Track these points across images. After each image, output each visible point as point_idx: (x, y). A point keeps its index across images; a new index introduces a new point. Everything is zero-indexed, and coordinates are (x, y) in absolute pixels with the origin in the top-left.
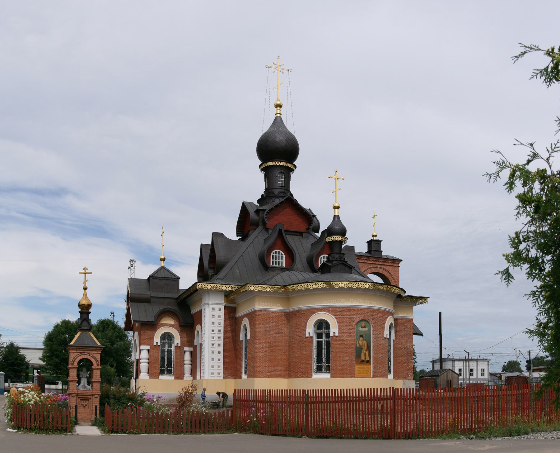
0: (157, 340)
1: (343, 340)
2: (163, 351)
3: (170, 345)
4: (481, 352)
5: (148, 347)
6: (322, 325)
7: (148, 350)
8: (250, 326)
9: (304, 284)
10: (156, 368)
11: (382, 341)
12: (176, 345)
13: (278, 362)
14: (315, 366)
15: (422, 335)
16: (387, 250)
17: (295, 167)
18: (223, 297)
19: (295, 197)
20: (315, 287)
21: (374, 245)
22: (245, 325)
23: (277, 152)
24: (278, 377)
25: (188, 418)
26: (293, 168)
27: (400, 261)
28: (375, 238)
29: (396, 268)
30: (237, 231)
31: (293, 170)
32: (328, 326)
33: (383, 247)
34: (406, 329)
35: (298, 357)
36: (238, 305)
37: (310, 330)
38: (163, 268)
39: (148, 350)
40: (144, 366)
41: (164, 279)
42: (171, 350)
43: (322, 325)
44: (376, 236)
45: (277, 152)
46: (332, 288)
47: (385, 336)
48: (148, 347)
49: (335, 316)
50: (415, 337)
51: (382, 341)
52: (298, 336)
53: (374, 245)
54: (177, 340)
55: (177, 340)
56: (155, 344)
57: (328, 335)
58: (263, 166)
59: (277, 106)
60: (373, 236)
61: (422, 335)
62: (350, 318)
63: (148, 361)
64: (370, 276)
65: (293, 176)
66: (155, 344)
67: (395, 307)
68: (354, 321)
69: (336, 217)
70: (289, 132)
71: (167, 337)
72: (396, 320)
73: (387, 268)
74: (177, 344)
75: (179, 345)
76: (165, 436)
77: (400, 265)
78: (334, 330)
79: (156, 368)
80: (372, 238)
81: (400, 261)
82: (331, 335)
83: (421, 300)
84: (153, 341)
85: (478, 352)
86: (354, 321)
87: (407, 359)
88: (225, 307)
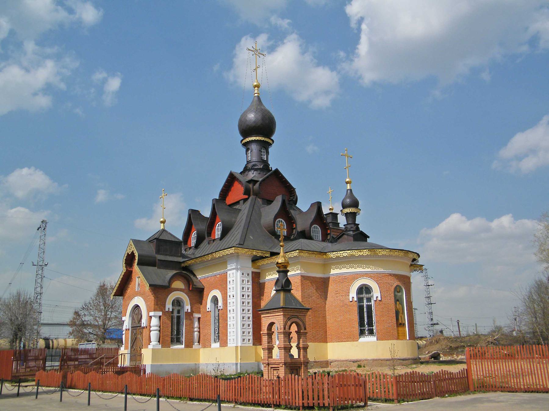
0: (169, 306)
2: (172, 318)
3: (369, 300)
6: (364, 290)
9: (350, 251)
20: (361, 254)
24: (320, 342)
25: (211, 388)
35: (341, 321)
36: (262, 270)
37: (353, 294)
38: (164, 230)
39: (160, 317)
40: (154, 335)
43: (364, 290)
46: (376, 255)
52: (340, 300)
54: (188, 308)
56: (167, 310)
58: (244, 142)
60: (330, 209)
62: (389, 284)
66: (167, 310)
68: (392, 286)
71: (178, 303)
74: (377, 297)
75: (379, 298)
78: (376, 293)
84: (165, 307)
88: (252, 272)
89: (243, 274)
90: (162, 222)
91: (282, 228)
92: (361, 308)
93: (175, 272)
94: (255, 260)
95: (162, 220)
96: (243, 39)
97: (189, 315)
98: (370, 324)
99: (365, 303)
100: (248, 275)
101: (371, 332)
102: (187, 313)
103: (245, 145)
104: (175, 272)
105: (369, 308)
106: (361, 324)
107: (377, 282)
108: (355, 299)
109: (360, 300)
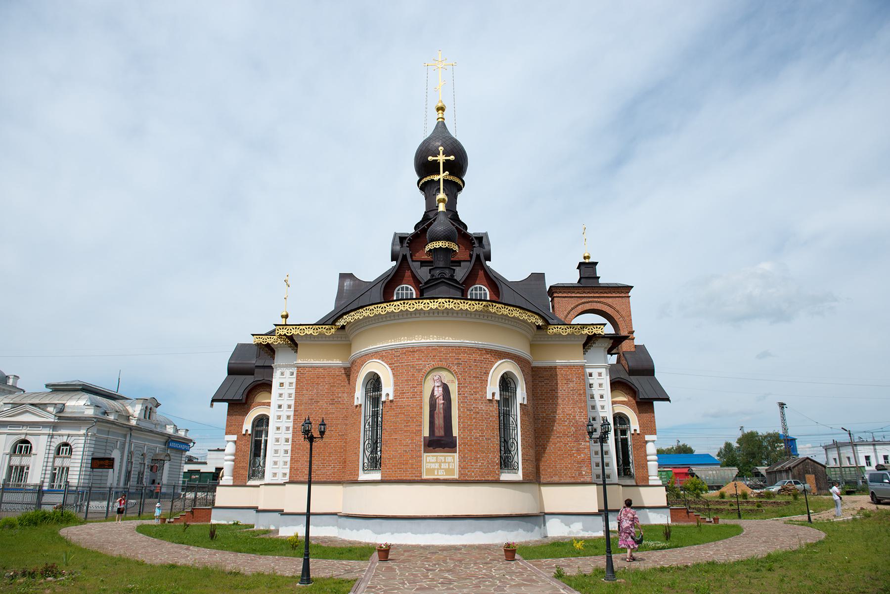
1: (401, 407)
5: (234, 438)
7: (235, 442)
10: (243, 468)
11: (483, 407)
12: (633, 432)
13: (330, 453)
14: (363, 458)
15: (668, 399)
16: (605, 276)
23: (442, 166)
26: (460, 183)
28: (587, 261)
29: (624, 300)
33: (599, 271)
34: (571, 385)
37: (359, 395)
39: (235, 442)
42: (627, 439)
44: (589, 257)
45: (442, 166)
48: (234, 438)
49: (390, 364)
51: (483, 407)
59: (438, 109)
60: (585, 258)
61: (668, 399)
63: (233, 458)
70: (453, 138)
73: (609, 301)
76: (414, 543)
77: (630, 294)
78: (388, 390)
79: (243, 468)
80: (583, 260)
86: (420, 370)
87: (577, 441)
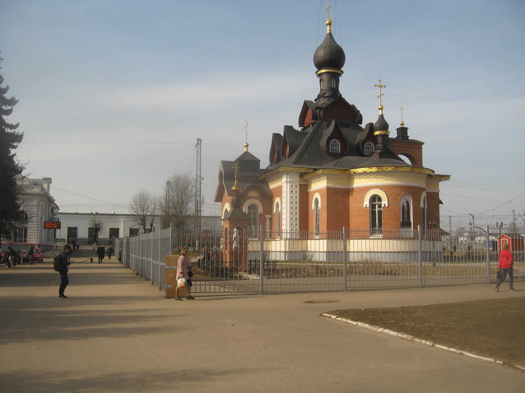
4: (483, 215)
8: (321, 199)
16: (412, 135)
17: (343, 72)
18: (298, 176)
19: (343, 96)
21: (403, 131)
22: (317, 199)
27: (423, 143)
30: (299, 123)
31: (340, 75)
32: (380, 199)
37: (366, 203)
38: (247, 153)
41: (248, 162)
43: (375, 198)
47: (421, 207)
50: (440, 205)
53: (403, 131)
54: (260, 210)
55: (260, 210)
57: (380, 206)
58: (319, 72)
64: (401, 156)
65: (341, 79)
67: (427, 183)
69: (382, 117)
71: (253, 207)
72: (427, 193)
75: (262, 213)
78: (385, 202)
81: (423, 143)
82: (383, 206)
83: (446, 177)
85: (480, 215)
89: (292, 186)
90: (379, 109)
91: (337, 146)
92: (373, 213)
93: (248, 185)
94: (302, 175)
95: (380, 107)
96: (13, 151)
97: (262, 216)
98: (380, 225)
99: (377, 209)
100: (296, 186)
101: (380, 232)
102: (260, 214)
103: (319, 75)
104: (248, 185)
105: (380, 212)
106: (373, 225)
107: (385, 192)
108: (368, 206)
109: (373, 206)
